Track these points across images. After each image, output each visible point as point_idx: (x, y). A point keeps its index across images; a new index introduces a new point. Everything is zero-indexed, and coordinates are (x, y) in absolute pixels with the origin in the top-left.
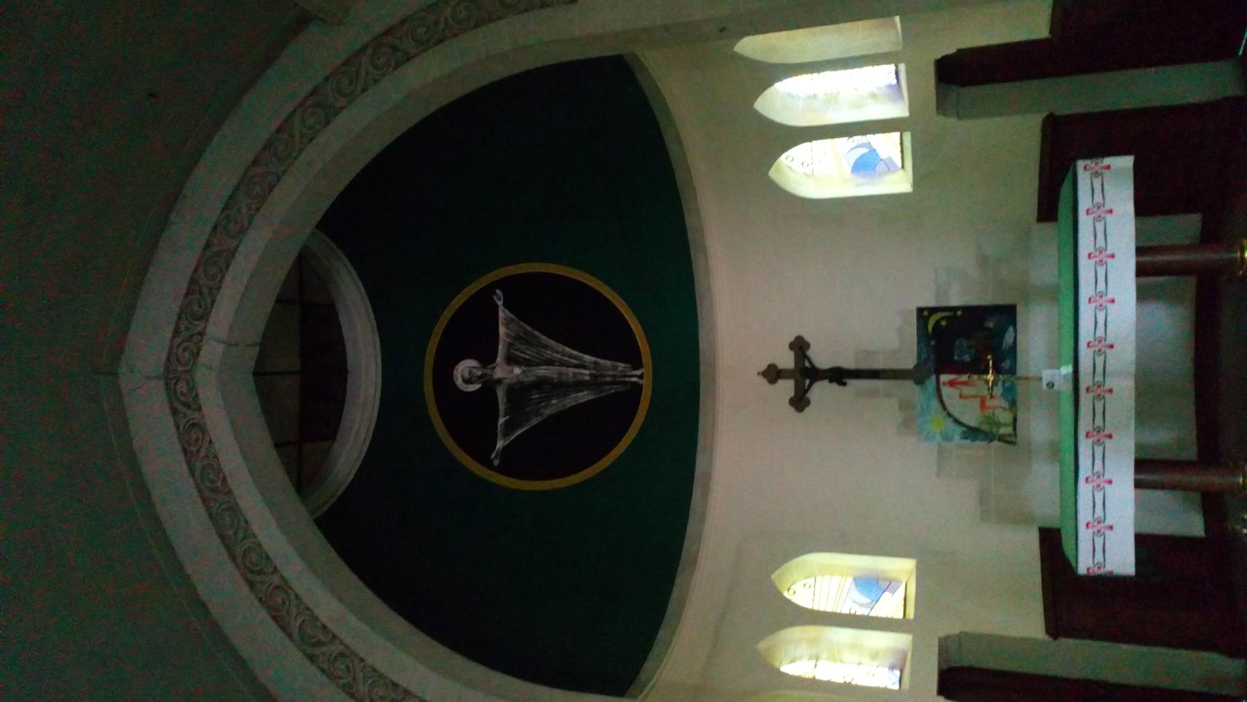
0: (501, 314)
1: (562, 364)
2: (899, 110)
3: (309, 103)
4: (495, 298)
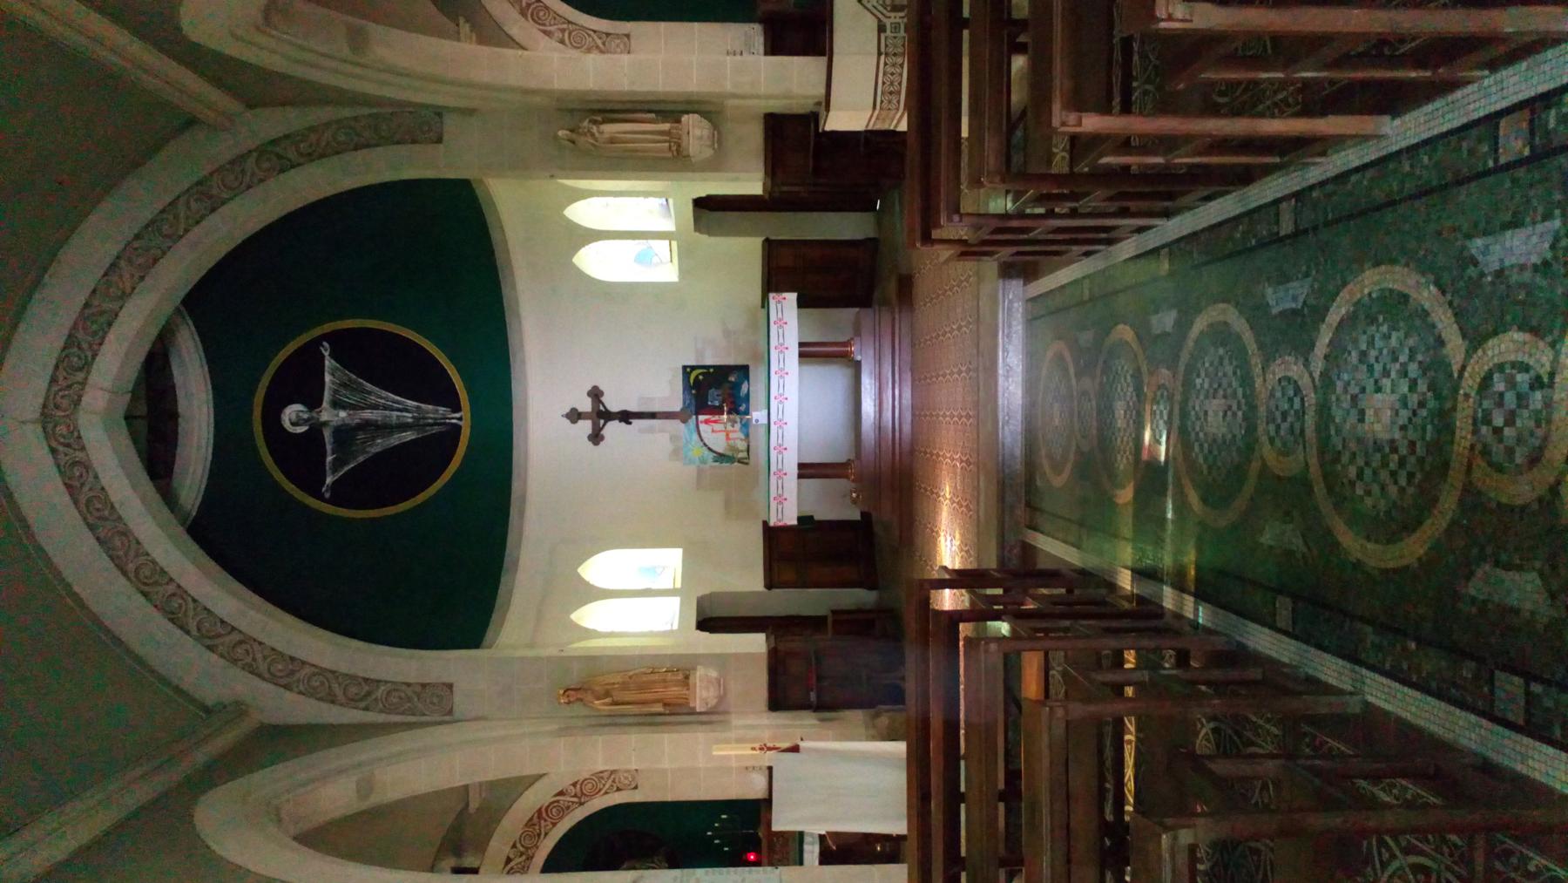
0: (327, 363)
1: (385, 408)
2: (669, 225)
3: (195, 190)
4: (322, 349)
